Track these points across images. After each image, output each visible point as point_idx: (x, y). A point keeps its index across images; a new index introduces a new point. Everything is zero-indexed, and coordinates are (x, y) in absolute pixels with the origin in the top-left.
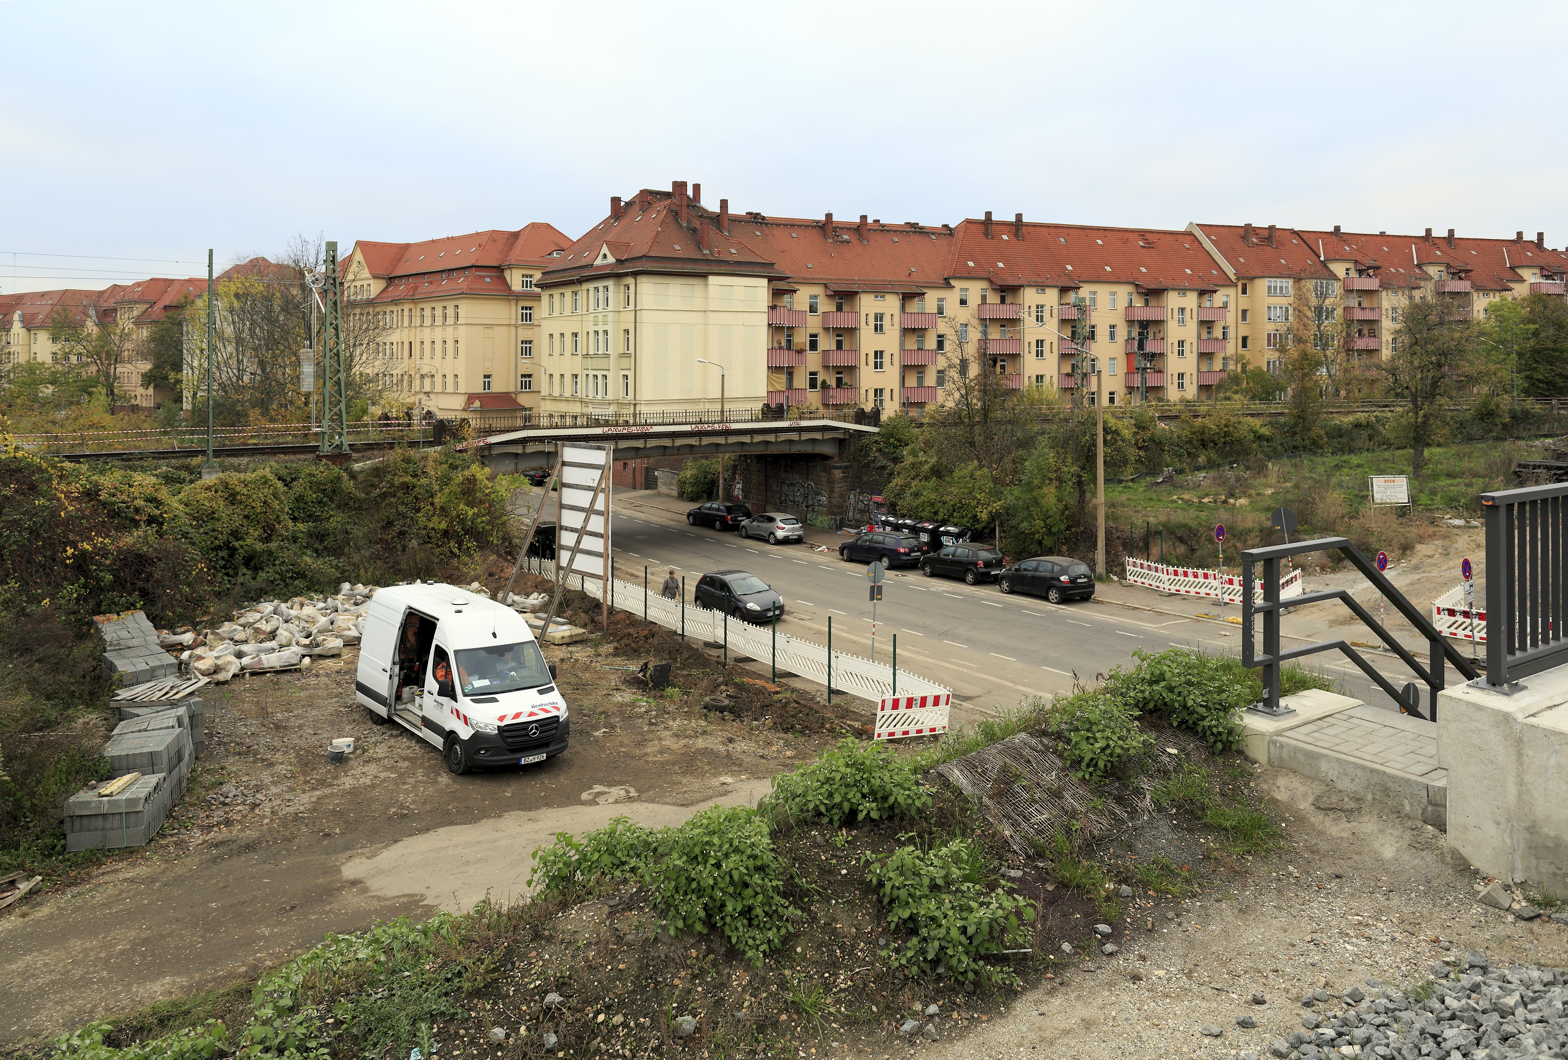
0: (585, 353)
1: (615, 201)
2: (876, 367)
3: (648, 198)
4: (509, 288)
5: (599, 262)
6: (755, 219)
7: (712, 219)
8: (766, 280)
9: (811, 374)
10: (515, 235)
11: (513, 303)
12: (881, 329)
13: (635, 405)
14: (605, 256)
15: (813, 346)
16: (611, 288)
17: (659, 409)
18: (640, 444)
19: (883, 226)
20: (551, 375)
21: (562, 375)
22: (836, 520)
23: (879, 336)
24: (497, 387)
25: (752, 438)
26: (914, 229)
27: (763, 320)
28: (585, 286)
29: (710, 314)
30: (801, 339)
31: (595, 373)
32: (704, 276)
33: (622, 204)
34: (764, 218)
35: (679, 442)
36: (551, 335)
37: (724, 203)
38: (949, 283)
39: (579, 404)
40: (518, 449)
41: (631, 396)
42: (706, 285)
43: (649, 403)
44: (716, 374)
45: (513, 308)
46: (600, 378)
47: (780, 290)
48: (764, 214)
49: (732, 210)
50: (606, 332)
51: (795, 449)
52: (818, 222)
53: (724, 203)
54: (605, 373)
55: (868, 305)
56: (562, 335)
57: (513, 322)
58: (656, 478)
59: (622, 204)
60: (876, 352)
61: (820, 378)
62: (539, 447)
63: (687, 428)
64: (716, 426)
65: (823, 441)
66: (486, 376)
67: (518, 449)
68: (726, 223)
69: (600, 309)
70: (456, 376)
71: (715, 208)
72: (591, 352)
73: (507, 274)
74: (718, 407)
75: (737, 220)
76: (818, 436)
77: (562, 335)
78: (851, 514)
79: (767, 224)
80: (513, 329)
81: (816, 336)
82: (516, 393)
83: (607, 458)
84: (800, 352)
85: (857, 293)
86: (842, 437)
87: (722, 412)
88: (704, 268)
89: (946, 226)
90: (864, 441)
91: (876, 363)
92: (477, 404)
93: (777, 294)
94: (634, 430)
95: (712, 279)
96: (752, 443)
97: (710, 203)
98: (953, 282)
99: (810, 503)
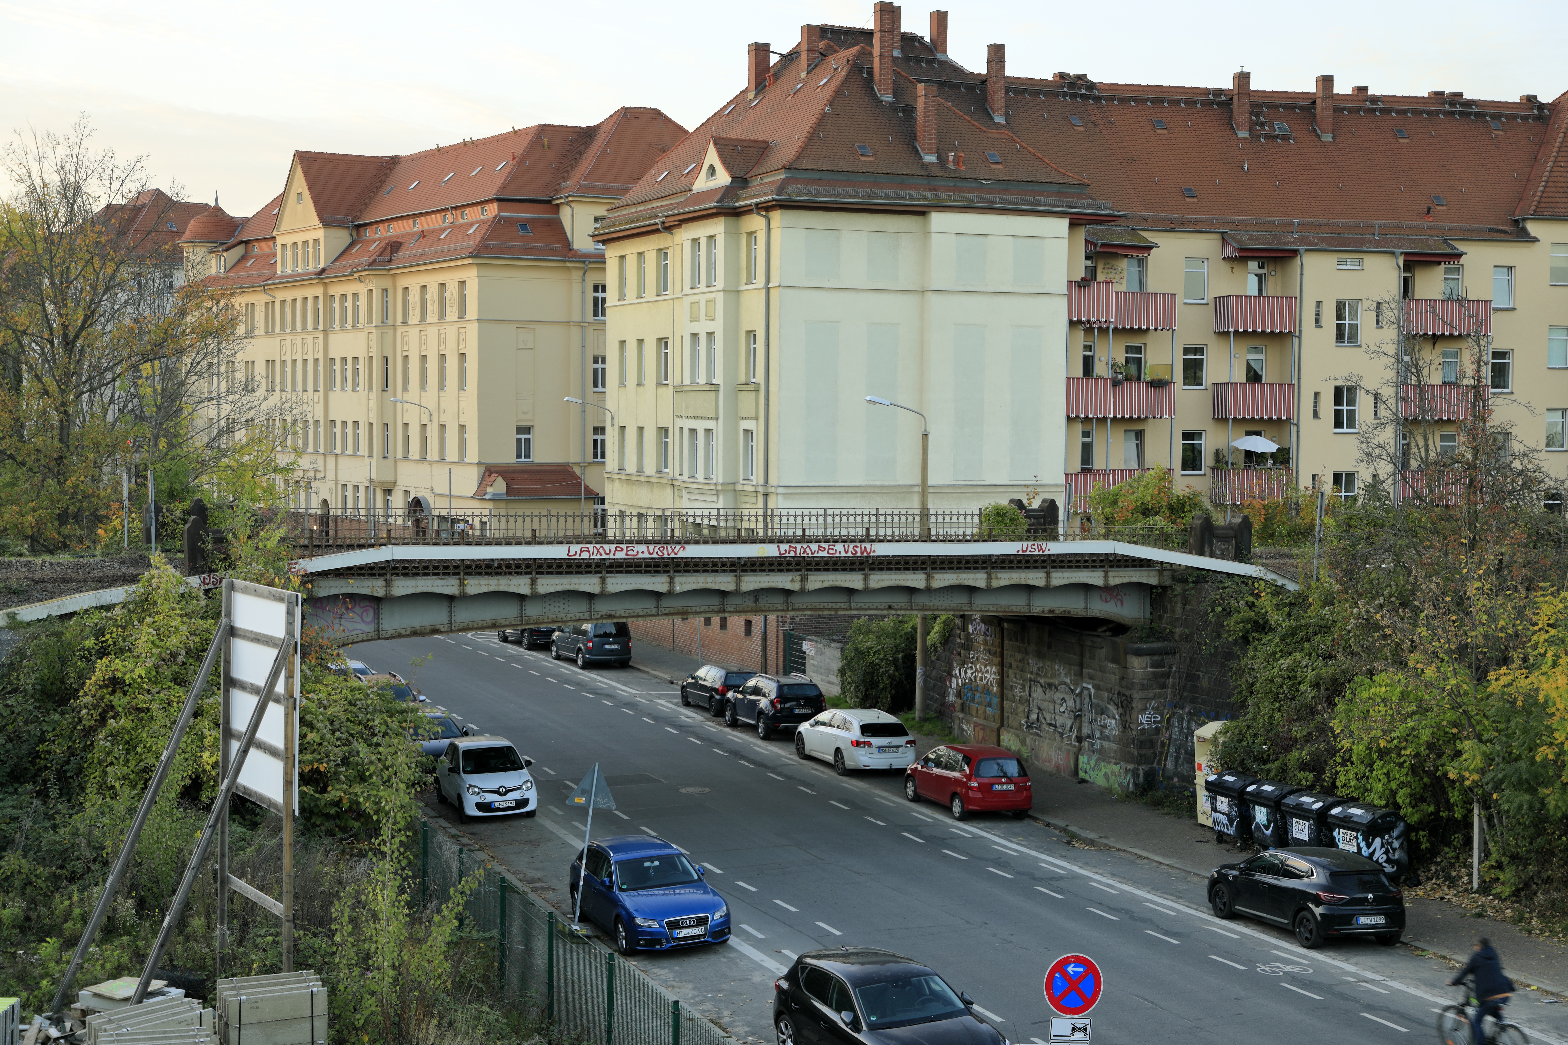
0: (678, 382)
1: (760, 51)
2: (1338, 424)
3: (825, 39)
4: (566, 244)
5: (701, 184)
6: (1073, 89)
7: (970, 88)
8: (1064, 223)
9: (1187, 436)
10: (587, 134)
11: (576, 275)
12: (1353, 338)
13: (766, 495)
14: (712, 170)
15: (1193, 371)
16: (721, 240)
17: (814, 505)
18: (658, 583)
19: (1375, 99)
20: (622, 428)
21: (641, 429)
22: (1135, 774)
23: (1347, 353)
24: (544, 453)
25: (929, 578)
26: (1450, 108)
27: (1058, 312)
28: (685, 235)
29: (933, 299)
30: (1163, 356)
31: (693, 424)
32: (921, 212)
33: (774, 59)
34: (1092, 86)
35: (752, 582)
36: (623, 343)
37: (997, 53)
38: (1524, 231)
39: (669, 491)
40: (375, 587)
41: (758, 478)
42: (926, 233)
43: (793, 491)
44: (907, 429)
45: (577, 287)
46: (701, 434)
47: (1108, 246)
48: (1094, 78)
49: (1014, 69)
50: (710, 335)
51: (1040, 606)
52: (1218, 92)
53: (997, 53)
54: (710, 424)
55: (1321, 278)
56: (641, 341)
57: (576, 317)
58: (803, 656)
59: (774, 59)
60: (1338, 391)
61: (1209, 445)
62: (354, 586)
63: (770, 551)
64: (839, 547)
65: (1107, 590)
66: (521, 430)
67: (375, 587)
68: (998, 98)
69: (702, 287)
70: (462, 427)
71: (975, 62)
72: (687, 381)
73: (565, 214)
74: (914, 505)
75: (1026, 90)
76: (1095, 578)
77: (641, 341)
78: (1170, 765)
79: (1097, 99)
80: (576, 332)
81: (1199, 350)
82: (584, 465)
83: (290, 623)
84: (1158, 384)
85: (1295, 252)
86: (1154, 581)
87: (925, 514)
88: (910, 196)
89: (1531, 100)
90: (1212, 594)
91: (1338, 414)
92: (500, 486)
93: (1100, 254)
94: (642, 552)
95: (939, 220)
96: (802, 592)
97: (967, 54)
98: (1532, 228)
99: (1085, 731)
